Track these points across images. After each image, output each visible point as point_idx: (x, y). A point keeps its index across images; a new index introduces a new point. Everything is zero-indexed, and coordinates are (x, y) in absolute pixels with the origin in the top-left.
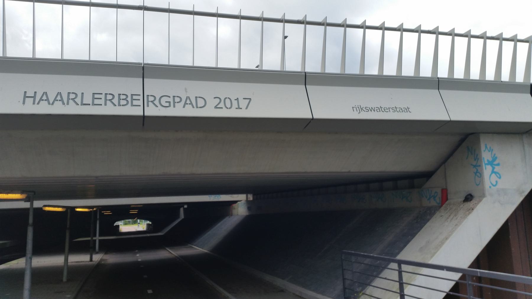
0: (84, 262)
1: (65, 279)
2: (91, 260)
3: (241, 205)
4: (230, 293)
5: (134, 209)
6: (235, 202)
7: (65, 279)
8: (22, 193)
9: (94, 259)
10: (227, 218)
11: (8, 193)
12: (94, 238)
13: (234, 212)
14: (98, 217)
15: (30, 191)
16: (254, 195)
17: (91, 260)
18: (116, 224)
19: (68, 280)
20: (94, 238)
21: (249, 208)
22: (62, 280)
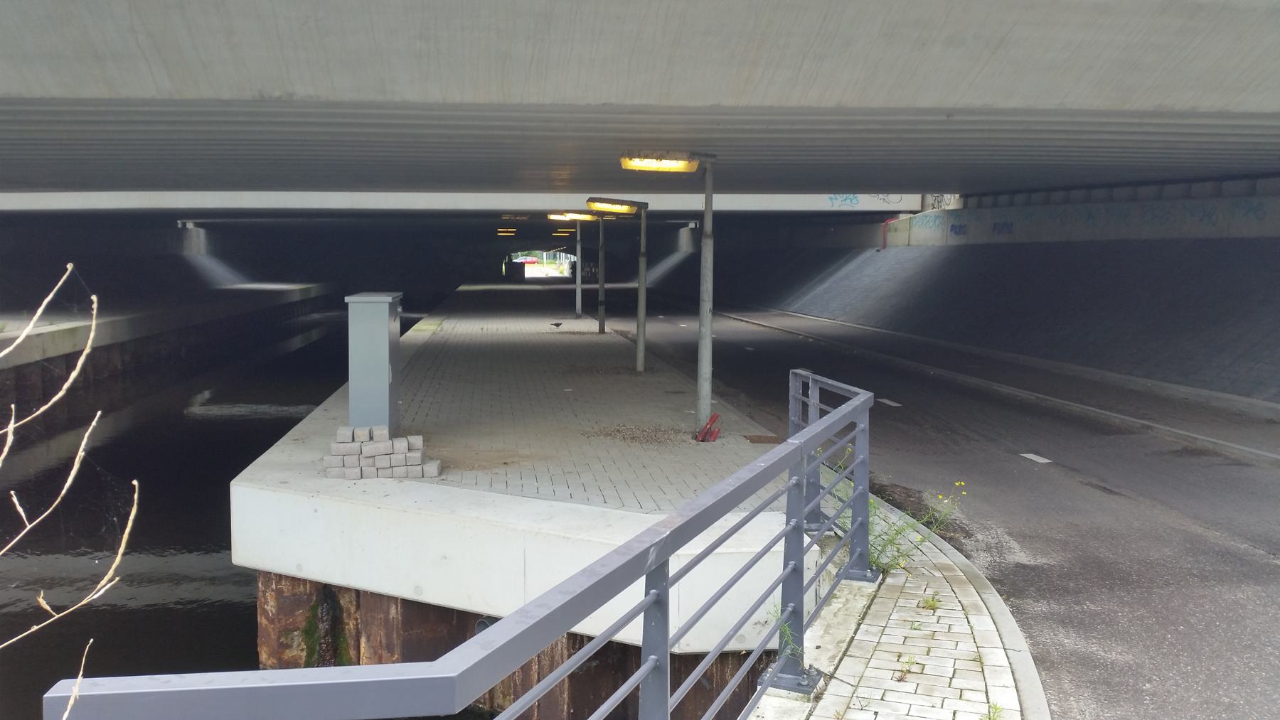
0: (584, 333)
1: (640, 365)
2: (602, 331)
3: (920, 227)
4: (1248, 395)
5: (507, 225)
6: (894, 214)
7: (640, 365)
8: (691, 156)
9: (607, 329)
10: (869, 253)
11: (660, 158)
12: (601, 298)
13: (891, 237)
14: (643, 249)
15: (707, 155)
16: (965, 197)
17: (602, 331)
18: (519, 258)
19: (648, 369)
20: (601, 298)
21: (957, 229)
22: (634, 369)
